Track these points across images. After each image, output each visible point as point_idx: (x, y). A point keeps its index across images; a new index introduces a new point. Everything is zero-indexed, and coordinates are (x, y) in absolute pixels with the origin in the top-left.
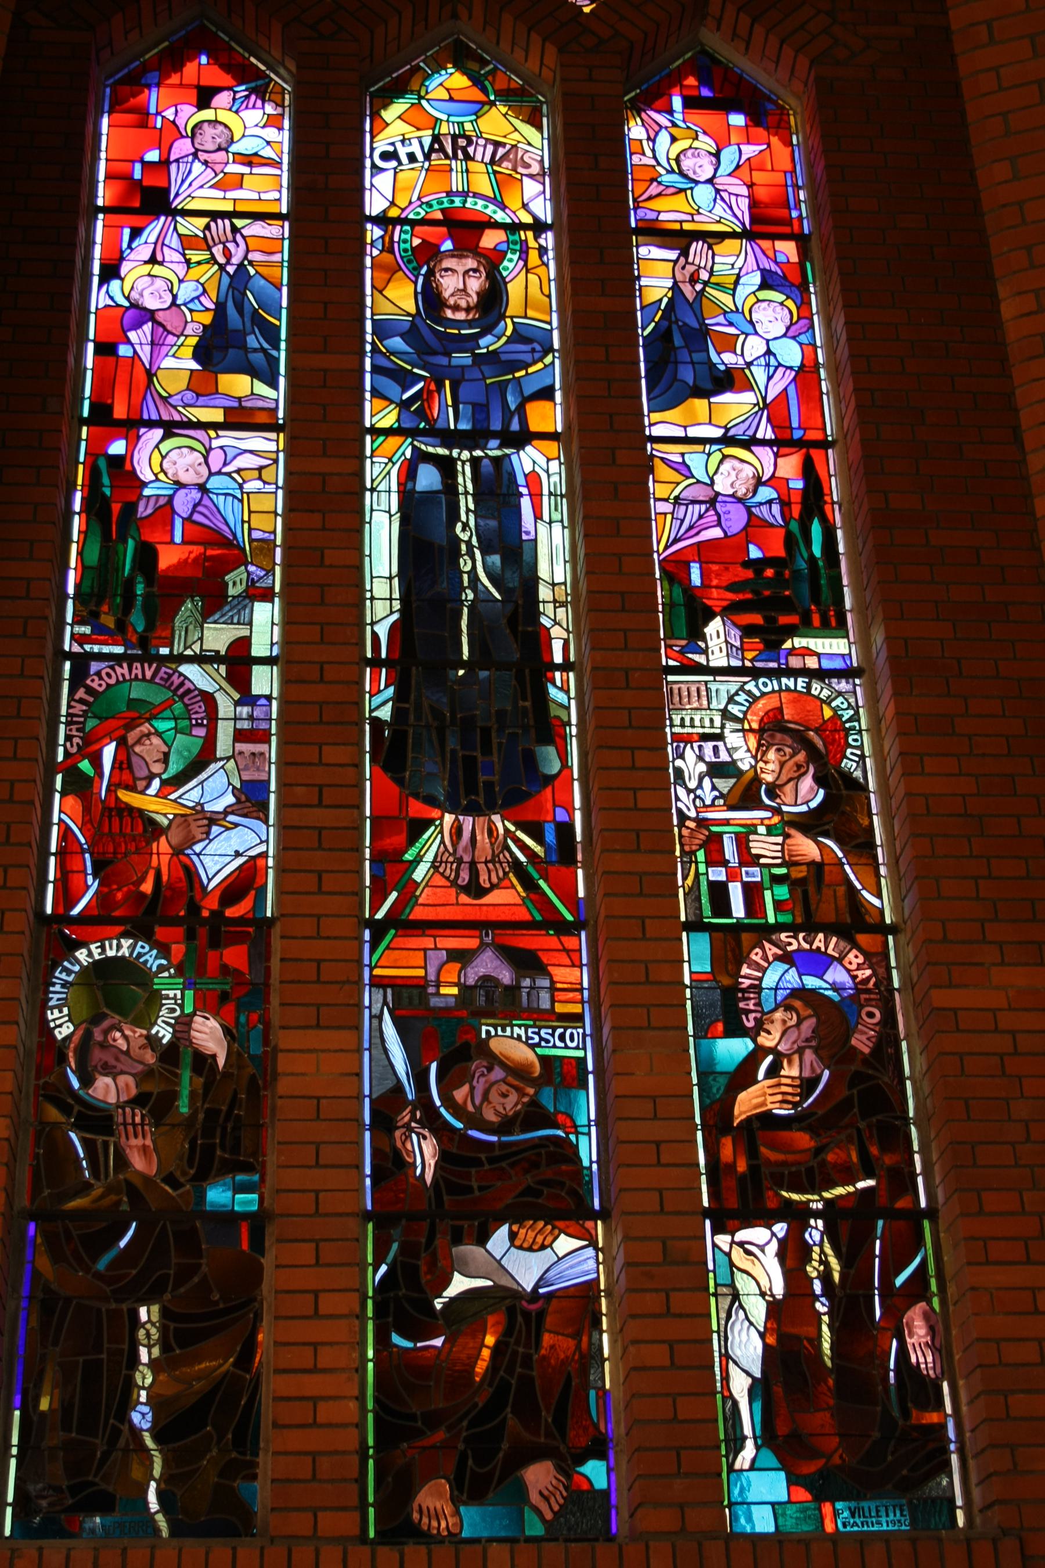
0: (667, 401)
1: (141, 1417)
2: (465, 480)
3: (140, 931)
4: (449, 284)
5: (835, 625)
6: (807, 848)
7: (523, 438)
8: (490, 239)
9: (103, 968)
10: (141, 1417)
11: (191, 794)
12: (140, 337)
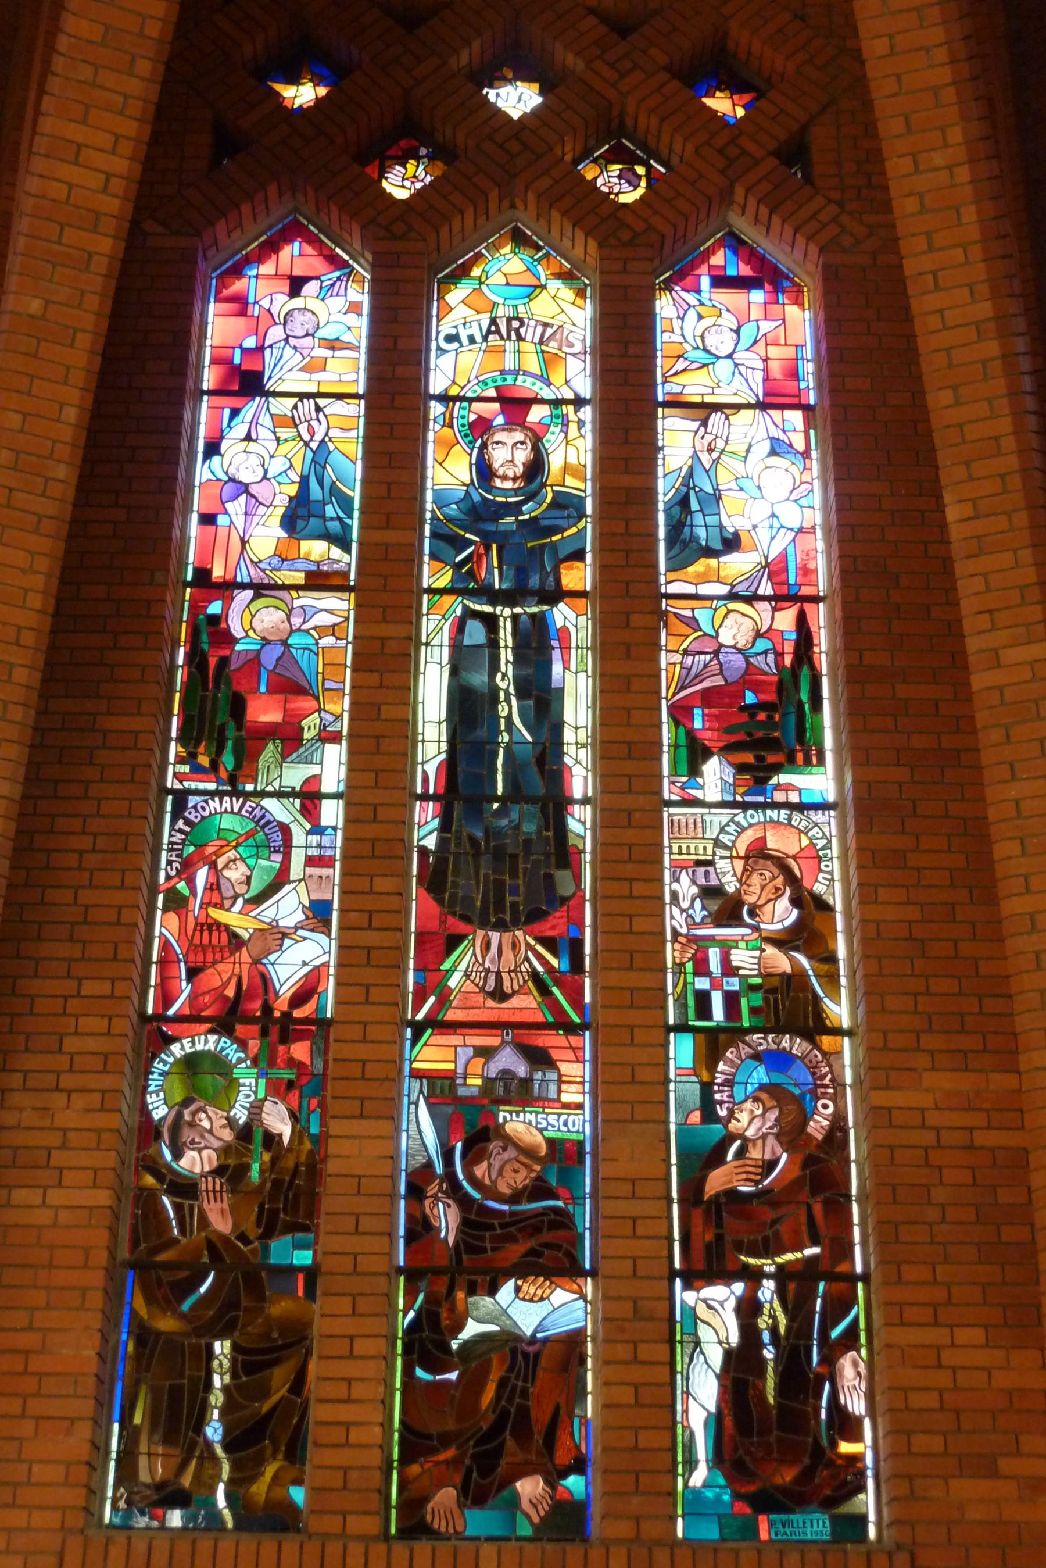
0: (677, 565)
1: (214, 1431)
2: (506, 635)
3: (224, 1026)
4: (499, 456)
5: (813, 758)
6: (780, 962)
7: (555, 595)
8: (537, 414)
9: (191, 1063)
10: (214, 1431)
11: (268, 911)
12: (236, 507)
